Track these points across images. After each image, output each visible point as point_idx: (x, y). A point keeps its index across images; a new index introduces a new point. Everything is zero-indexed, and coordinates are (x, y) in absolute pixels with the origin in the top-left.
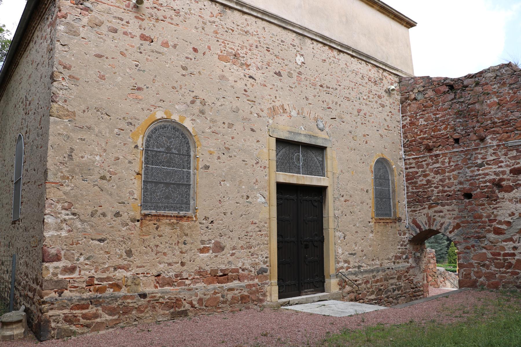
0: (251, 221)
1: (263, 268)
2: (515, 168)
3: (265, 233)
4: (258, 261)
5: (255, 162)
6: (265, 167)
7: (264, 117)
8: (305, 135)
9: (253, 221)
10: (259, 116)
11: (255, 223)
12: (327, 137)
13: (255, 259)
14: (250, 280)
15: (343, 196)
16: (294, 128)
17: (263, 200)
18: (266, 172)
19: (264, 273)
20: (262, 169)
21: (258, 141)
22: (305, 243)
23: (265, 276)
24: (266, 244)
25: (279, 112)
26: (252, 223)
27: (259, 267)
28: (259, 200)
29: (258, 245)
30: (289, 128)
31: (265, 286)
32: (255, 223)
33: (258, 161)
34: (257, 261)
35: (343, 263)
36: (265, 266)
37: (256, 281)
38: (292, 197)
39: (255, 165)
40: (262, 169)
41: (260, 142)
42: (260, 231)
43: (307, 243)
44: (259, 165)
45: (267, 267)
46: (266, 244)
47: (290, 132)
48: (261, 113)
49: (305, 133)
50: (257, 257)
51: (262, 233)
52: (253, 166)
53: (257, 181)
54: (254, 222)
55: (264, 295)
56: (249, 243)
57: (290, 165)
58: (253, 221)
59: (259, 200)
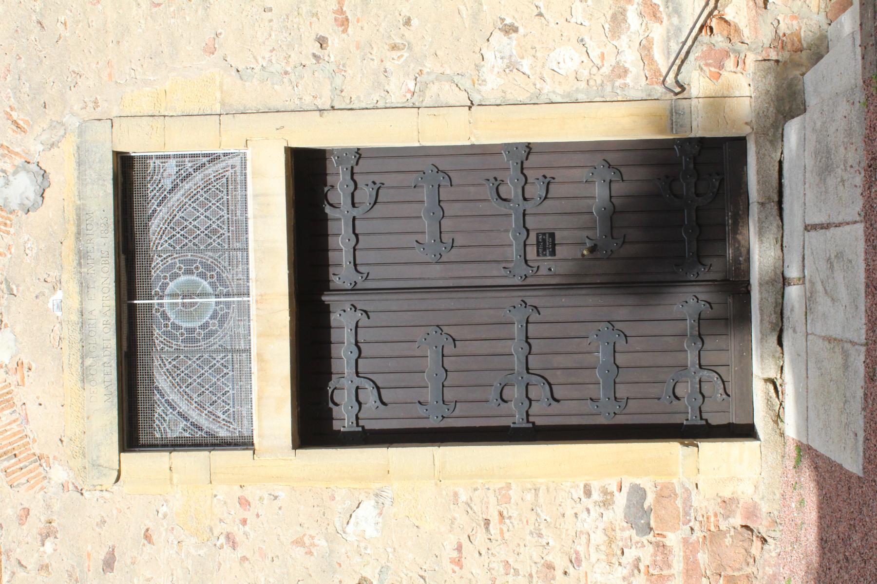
0: (449, 567)
1: (628, 507)
2: (125, 352)
3: (493, 500)
4: (600, 532)
5: (227, 549)
6: (244, 502)
7: (49, 507)
8: (84, 287)
9: (452, 561)
10: (48, 533)
11: (459, 548)
12: (68, 147)
13: (592, 549)
14: (669, 566)
15: (322, 42)
16: (65, 344)
17: (368, 508)
18: (261, 499)
19: (646, 505)
20: (249, 515)
21: (148, 537)
22: (532, 252)
23: (660, 497)
24: (537, 495)
25: (15, 427)
26: (458, 562)
27: (623, 529)
28: (371, 532)
29: (540, 535)
30: (71, 378)
31: (695, 504)
32: (459, 548)
33: (222, 540)
34: (598, 538)
35: (623, 42)
36: (621, 500)
37: (673, 539)
38: (347, 336)
39: (240, 552)
40: (249, 515)
41: (150, 525)
42: (487, 522)
43: (533, 239)
44: (238, 531)
45: (625, 489)
46: (537, 495)
47: (85, 376)
48: (36, 522)
49: (73, 287)
50: (584, 538)
51: (496, 514)
52: (244, 559)
53: (299, 542)
54: (455, 554)
55: (727, 504)
56: (531, 576)
57: (217, 351)
58: (452, 561)
59: (371, 532)
